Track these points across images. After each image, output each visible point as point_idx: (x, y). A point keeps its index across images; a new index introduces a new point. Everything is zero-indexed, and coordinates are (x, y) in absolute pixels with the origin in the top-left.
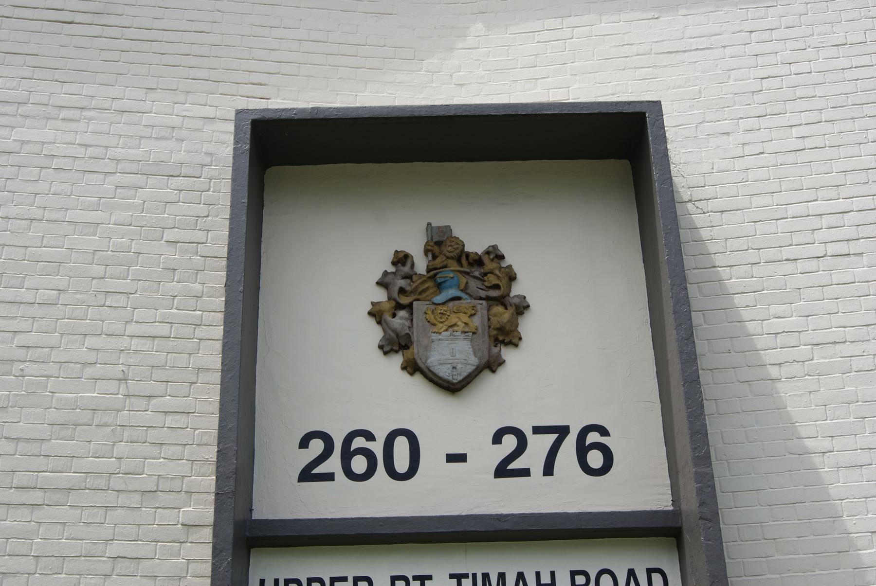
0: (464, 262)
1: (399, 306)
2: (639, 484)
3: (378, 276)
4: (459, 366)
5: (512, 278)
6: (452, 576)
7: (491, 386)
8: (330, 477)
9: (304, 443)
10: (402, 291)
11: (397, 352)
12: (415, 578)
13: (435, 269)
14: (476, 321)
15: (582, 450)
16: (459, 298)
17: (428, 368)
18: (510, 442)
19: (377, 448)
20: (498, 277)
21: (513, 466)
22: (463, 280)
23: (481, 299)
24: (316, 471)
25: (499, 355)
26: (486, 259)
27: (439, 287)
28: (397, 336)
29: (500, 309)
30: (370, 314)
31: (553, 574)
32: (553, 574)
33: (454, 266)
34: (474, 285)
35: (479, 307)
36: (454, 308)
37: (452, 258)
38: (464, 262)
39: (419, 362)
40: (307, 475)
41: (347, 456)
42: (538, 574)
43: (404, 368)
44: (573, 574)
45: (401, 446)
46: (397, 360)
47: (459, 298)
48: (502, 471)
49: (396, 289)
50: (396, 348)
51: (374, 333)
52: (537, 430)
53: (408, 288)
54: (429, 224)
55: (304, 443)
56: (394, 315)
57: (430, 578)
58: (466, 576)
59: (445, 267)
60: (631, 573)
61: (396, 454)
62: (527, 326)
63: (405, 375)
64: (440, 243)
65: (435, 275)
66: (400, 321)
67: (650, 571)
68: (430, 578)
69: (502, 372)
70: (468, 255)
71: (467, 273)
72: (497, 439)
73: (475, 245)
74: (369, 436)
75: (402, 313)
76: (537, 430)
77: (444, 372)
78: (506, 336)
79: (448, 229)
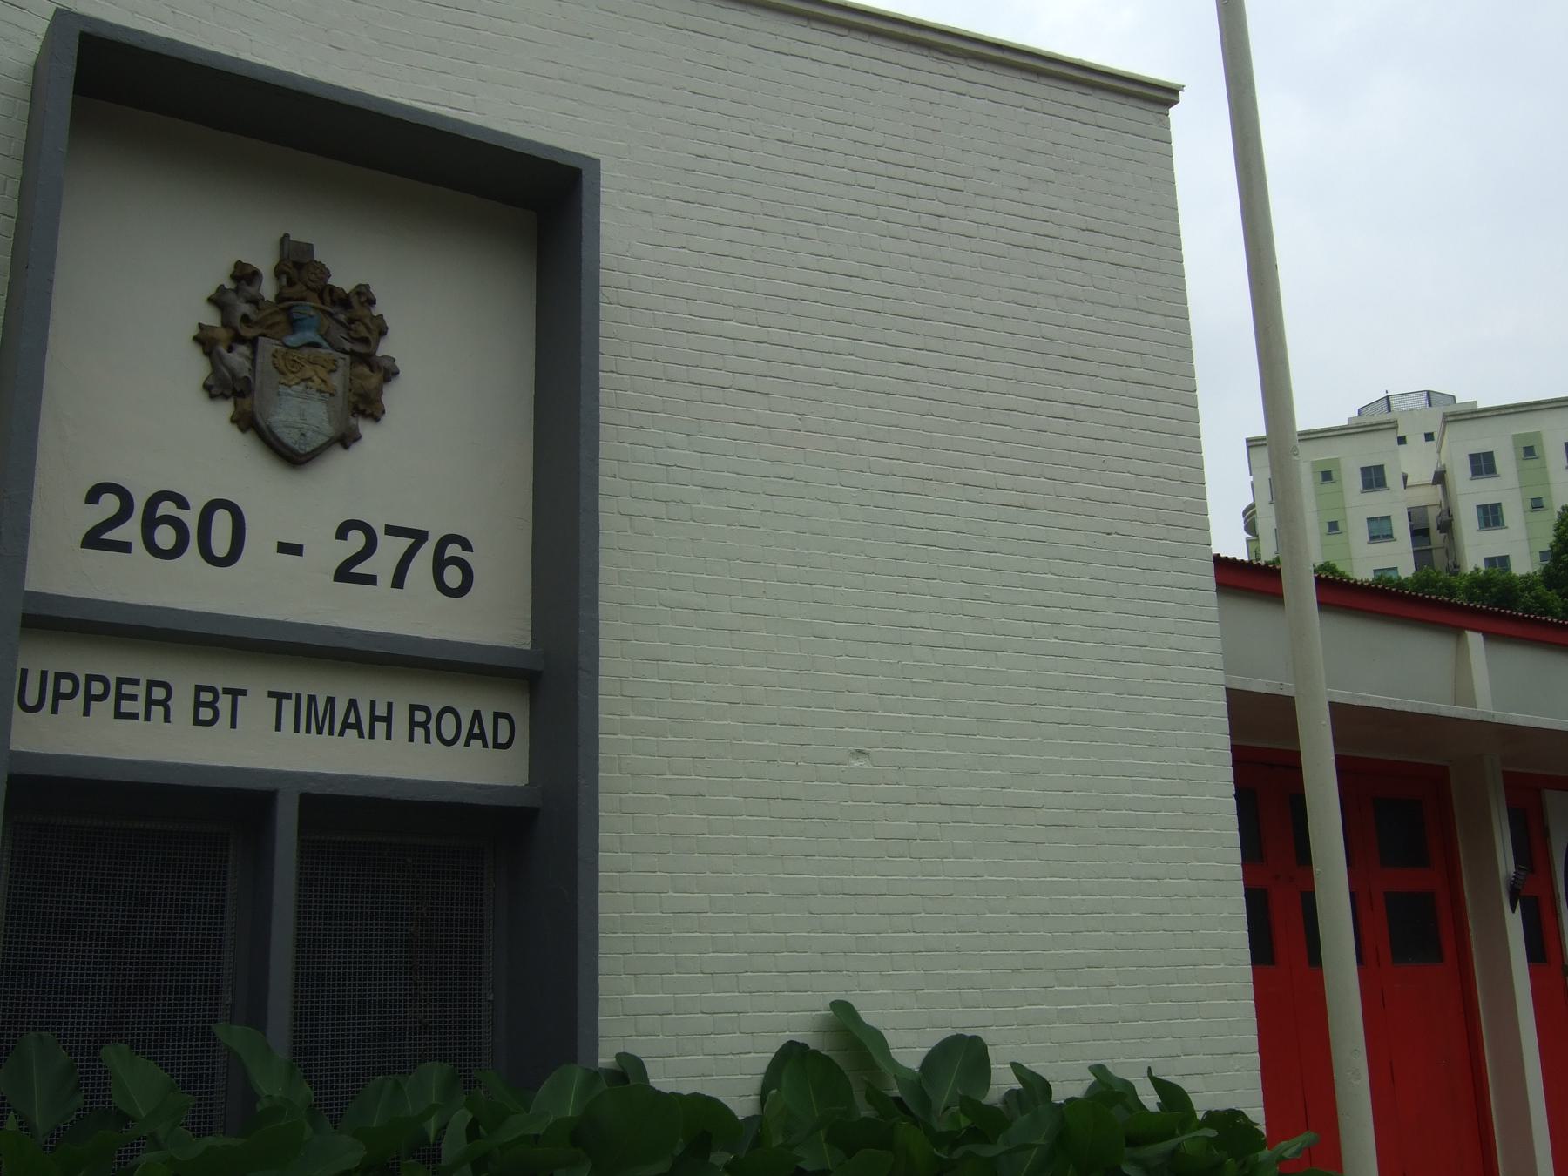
0: (328, 299)
1: (238, 339)
2: (493, 617)
3: (211, 290)
4: (309, 434)
5: (383, 332)
6: (271, 694)
7: (339, 463)
8: (125, 547)
9: (93, 496)
10: (245, 319)
11: (226, 397)
12: (226, 691)
13: (289, 299)
14: (337, 381)
15: (440, 563)
16: (317, 345)
17: (269, 427)
18: (357, 540)
19: (191, 519)
20: (368, 328)
21: (357, 569)
22: (327, 322)
23: (344, 351)
24: (106, 536)
25: (357, 428)
26: (354, 300)
27: (294, 325)
28: (234, 376)
29: (366, 370)
30: (196, 339)
31: (390, 705)
32: (390, 705)
33: (314, 301)
34: (338, 333)
35: (341, 362)
36: (293, 354)
37: (313, 290)
38: (328, 299)
39: (258, 417)
40: (93, 540)
41: (150, 523)
42: (373, 704)
43: (233, 421)
44: (413, 708)
45: (222, 523)
46: (226, 408)
47: (317, 345)
48: (344, 573)
49: (239, 315)
50: (228, 392)
51: (199, 368)
52: (391, 530)
53: (253, 317)
54: (286, 236)
55: (93, 496)
56: (230, 349)
57: (244, 693)
58: (288, 696)
59: (303, 299)
60: (477, 715)
61: (215, 533)
62: (392, 396)
63: (234, 431)
64: (297, 265)
65: (291, 307)
66: (238, 359)
67: (497, 716)
68: (244, 693)
69: (356, 448)
70: (332, 289)
71: (330, 314)
72: (342, 533)
73: (343, 279)
74: (182, 503)
75: (243, 349)
76: (391, 530)
77: (289, 437)
78: (367, 406)
79: (309, 249)
